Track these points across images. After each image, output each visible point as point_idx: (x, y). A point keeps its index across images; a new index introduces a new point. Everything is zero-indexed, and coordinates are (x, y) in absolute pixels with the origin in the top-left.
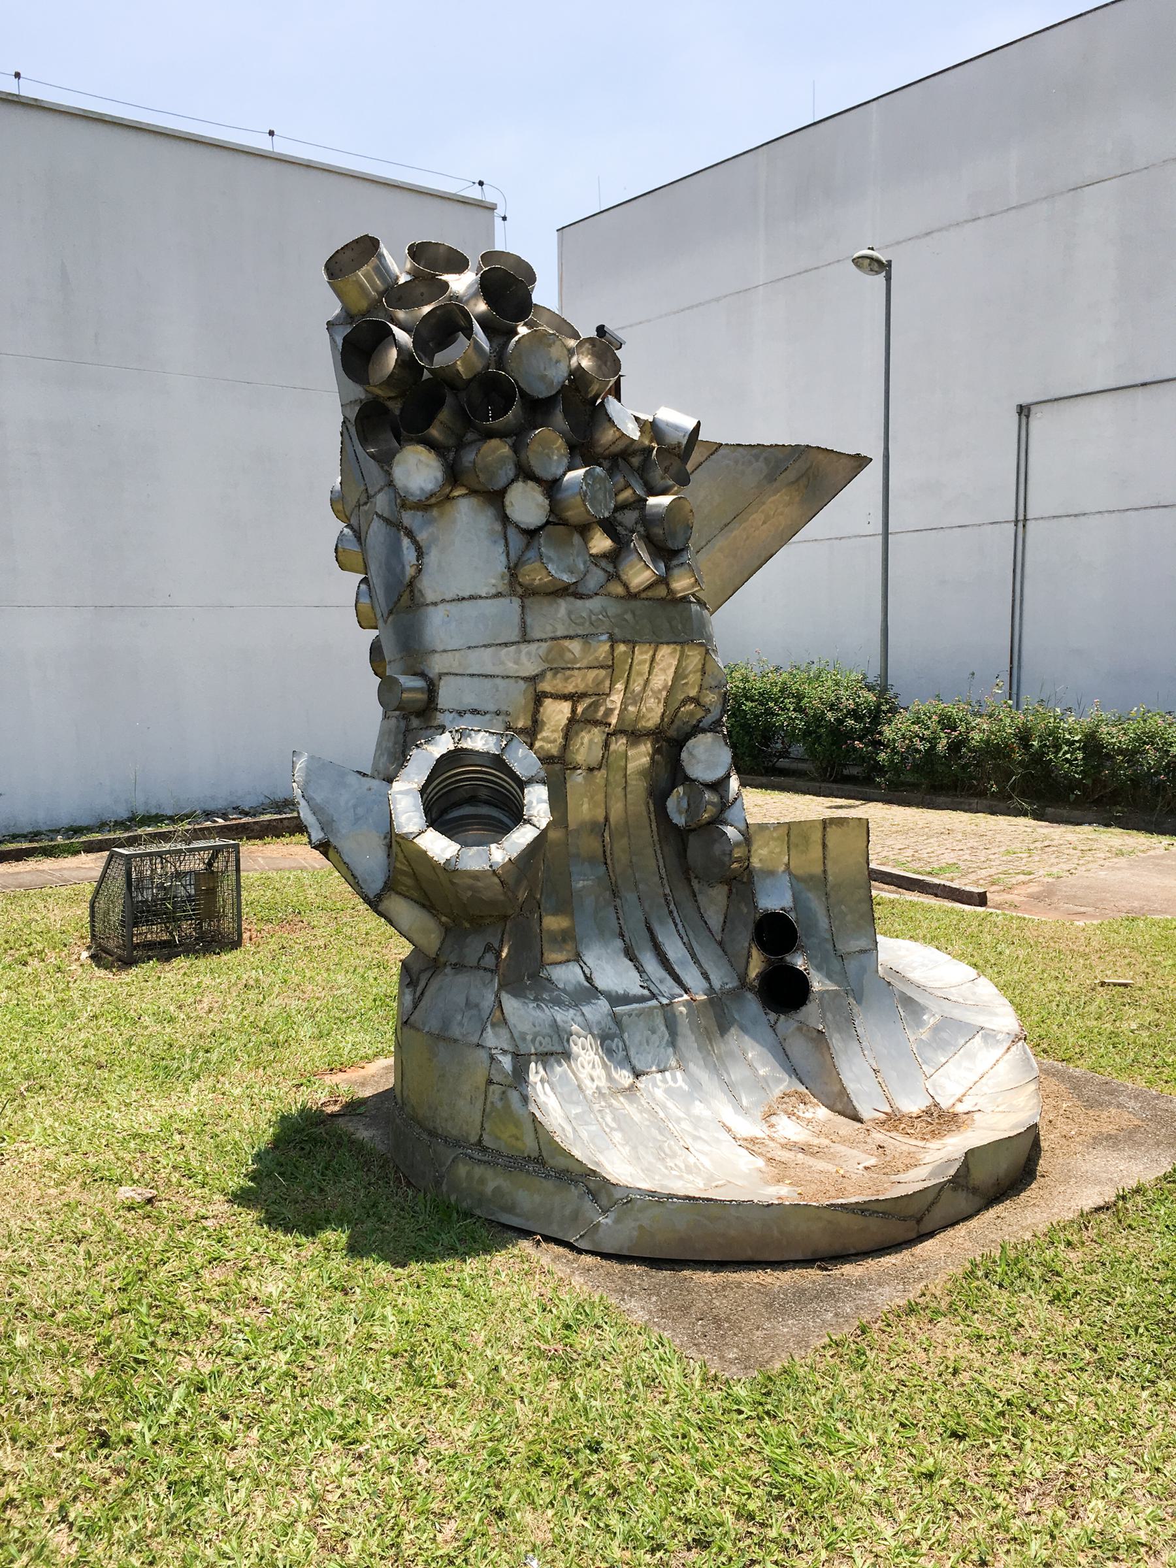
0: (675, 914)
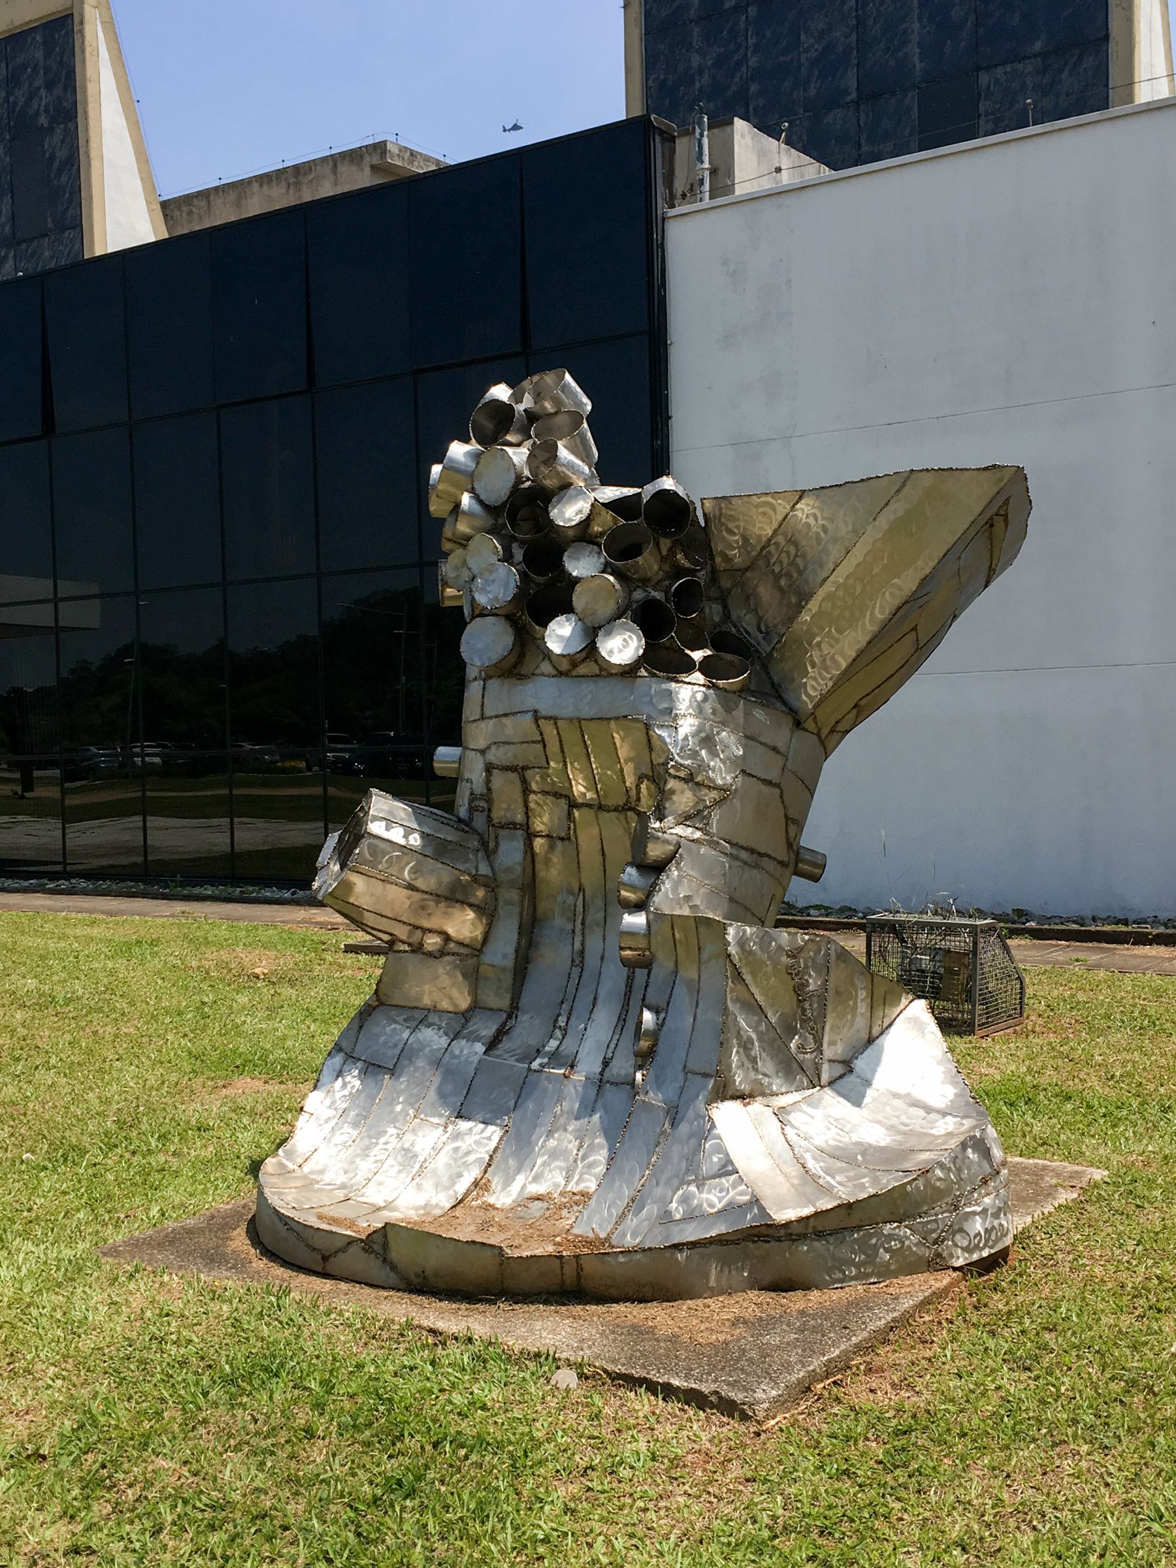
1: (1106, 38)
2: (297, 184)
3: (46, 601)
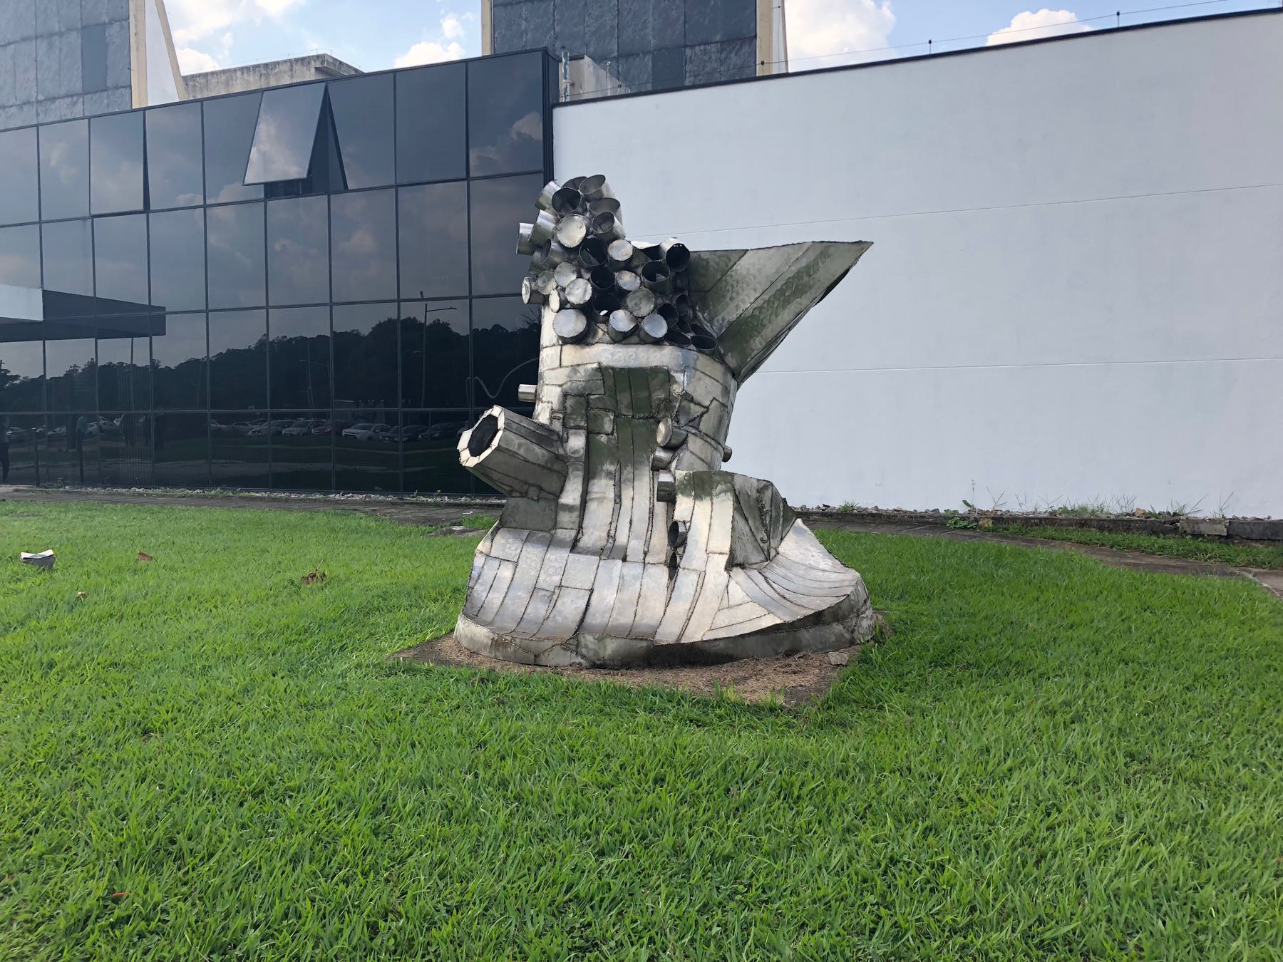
1: (755, 37)
2: (267, 76)
3: (325, 305)
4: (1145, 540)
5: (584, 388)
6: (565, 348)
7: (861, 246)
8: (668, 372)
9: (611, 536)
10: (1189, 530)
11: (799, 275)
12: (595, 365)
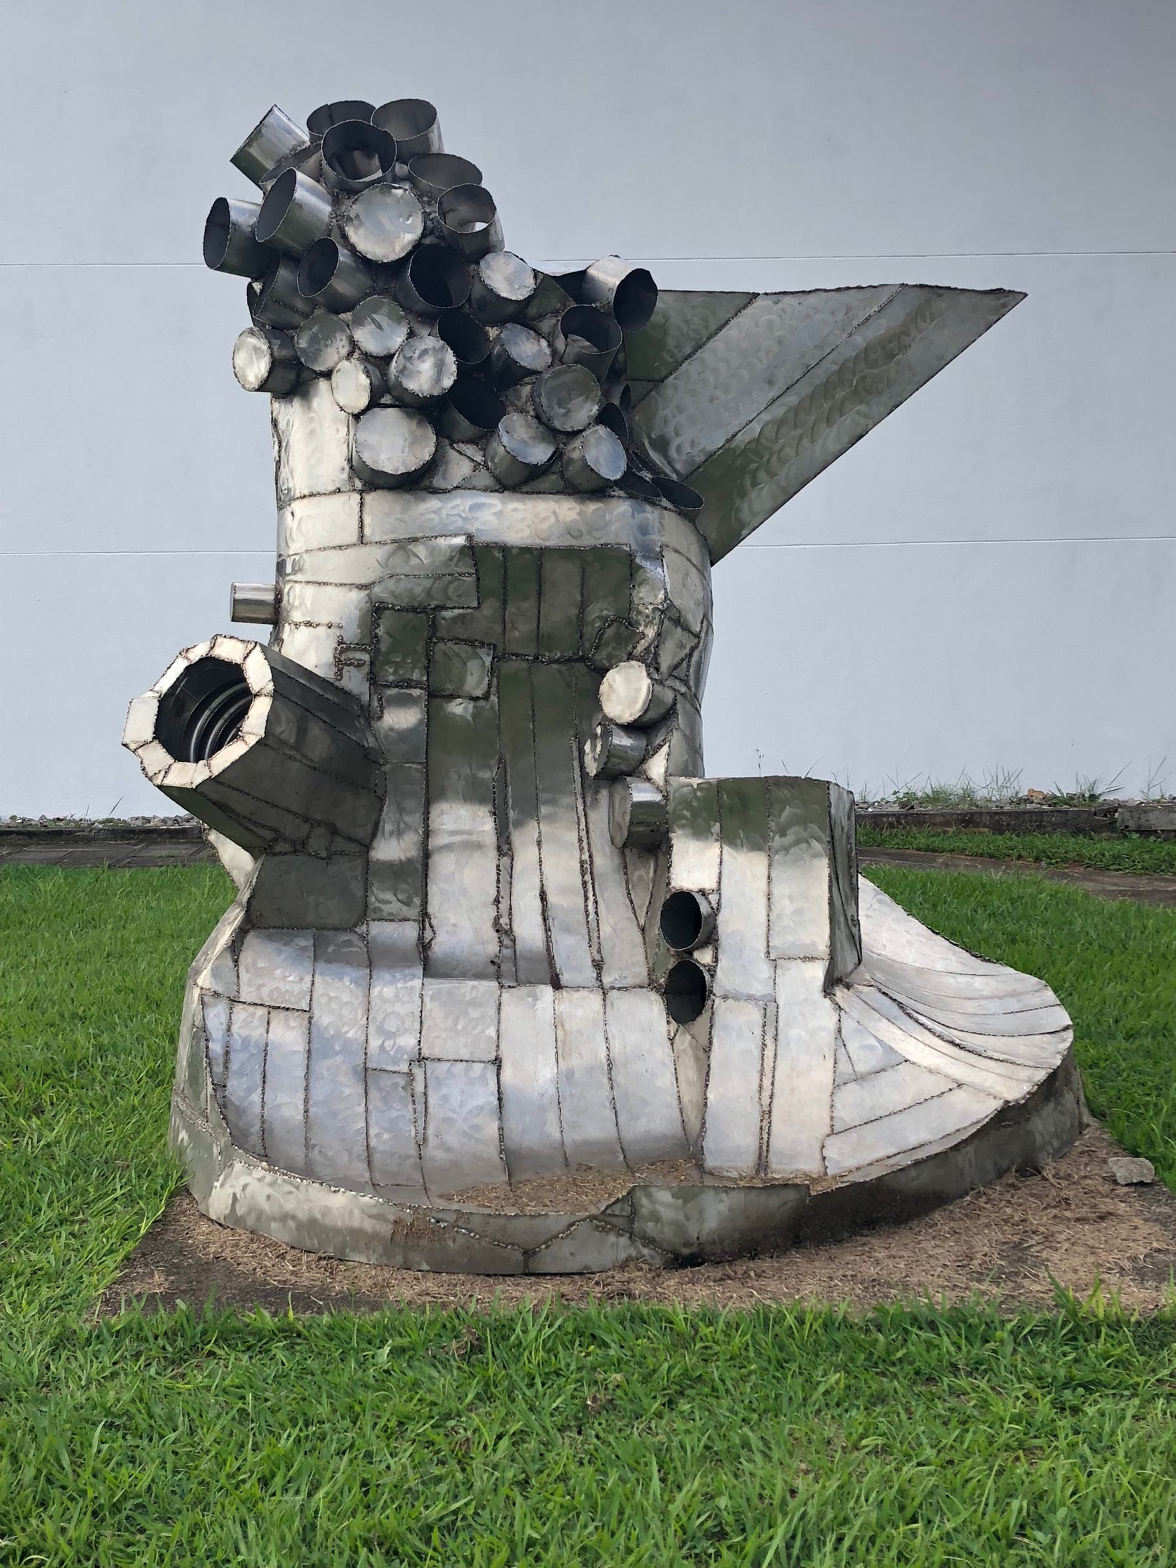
0: (590, 886)
4: (1073, 845)
5: (429, 593)
6: (369, 498)
7: (1002, 300)
8: (630, 557)
9: (504, 931)
10: (1132, 824)
11: (866, 355)
12: (460, 541)
